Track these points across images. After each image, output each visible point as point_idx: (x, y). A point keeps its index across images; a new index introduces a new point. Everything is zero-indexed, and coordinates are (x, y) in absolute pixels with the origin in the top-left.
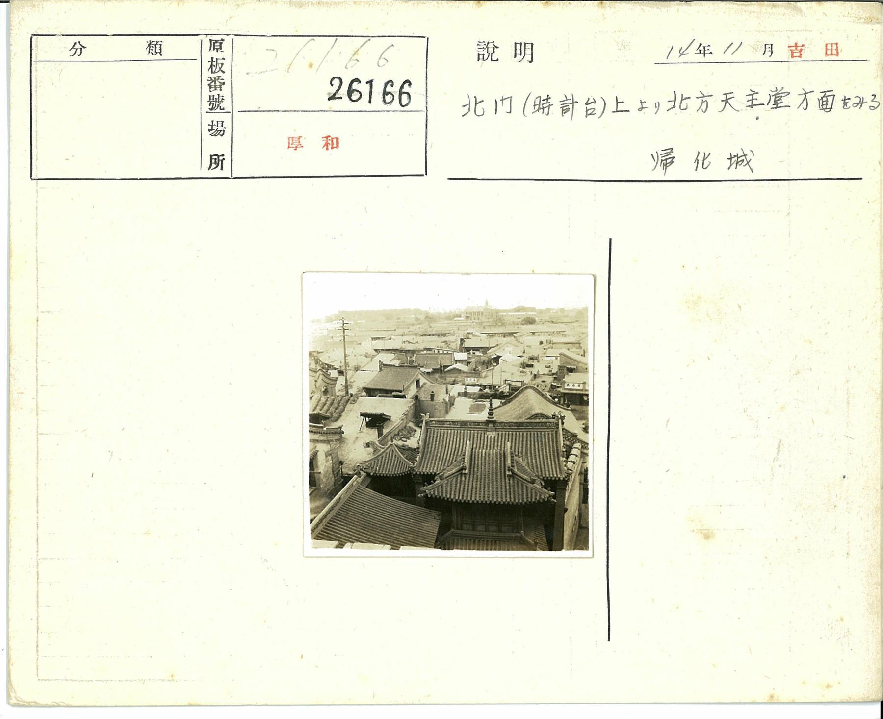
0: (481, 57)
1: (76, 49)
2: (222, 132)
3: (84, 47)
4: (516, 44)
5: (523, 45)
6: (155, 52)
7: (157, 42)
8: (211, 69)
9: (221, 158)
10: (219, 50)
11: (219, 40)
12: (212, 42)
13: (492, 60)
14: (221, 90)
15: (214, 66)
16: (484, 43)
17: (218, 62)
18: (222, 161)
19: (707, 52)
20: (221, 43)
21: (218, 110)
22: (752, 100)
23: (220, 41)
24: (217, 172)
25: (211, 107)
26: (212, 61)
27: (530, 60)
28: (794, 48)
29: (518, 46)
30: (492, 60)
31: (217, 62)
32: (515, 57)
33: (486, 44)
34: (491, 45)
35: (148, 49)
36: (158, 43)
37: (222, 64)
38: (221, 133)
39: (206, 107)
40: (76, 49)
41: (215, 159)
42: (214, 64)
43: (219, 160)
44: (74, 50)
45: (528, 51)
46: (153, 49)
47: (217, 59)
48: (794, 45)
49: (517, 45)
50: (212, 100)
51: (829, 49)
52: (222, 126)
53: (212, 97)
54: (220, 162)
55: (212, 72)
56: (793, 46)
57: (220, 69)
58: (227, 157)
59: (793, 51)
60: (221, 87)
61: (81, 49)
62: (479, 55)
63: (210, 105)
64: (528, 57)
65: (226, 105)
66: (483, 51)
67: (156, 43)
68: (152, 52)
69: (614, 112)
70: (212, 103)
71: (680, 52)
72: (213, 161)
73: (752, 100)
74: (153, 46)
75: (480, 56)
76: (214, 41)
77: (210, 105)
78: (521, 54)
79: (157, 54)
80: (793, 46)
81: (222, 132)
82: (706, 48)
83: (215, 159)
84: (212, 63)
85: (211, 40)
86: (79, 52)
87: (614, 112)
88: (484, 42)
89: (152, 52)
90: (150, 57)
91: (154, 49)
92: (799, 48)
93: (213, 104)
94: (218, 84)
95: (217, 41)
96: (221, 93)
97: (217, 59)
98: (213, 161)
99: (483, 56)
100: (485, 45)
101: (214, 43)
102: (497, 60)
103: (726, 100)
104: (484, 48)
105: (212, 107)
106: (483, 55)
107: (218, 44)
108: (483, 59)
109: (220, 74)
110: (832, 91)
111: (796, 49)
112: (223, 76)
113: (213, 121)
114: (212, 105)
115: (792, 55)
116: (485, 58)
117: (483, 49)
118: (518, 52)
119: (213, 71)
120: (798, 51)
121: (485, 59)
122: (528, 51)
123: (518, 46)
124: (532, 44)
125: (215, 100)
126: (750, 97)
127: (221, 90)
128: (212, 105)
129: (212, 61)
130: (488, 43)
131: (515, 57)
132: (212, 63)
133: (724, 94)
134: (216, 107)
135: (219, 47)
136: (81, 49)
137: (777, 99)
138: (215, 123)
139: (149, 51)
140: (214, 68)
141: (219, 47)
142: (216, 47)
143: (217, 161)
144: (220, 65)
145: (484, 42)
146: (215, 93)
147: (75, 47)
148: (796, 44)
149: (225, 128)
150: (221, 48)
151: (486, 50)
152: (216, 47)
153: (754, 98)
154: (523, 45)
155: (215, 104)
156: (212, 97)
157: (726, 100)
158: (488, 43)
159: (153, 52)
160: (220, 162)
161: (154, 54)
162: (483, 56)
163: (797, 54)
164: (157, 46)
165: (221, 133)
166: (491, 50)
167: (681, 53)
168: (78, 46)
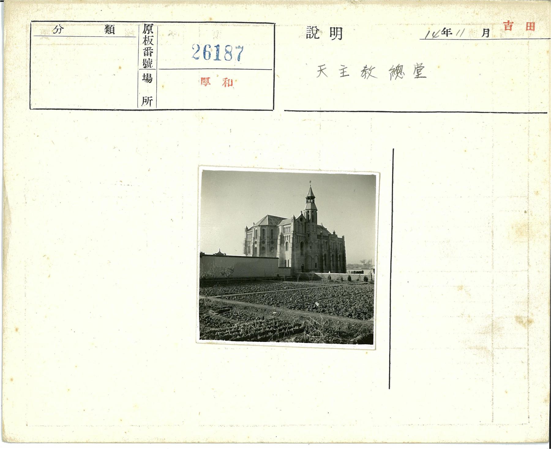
0: (308, 36)
1: (58, 29)
2: (150, 81)
3: (63, 28)
4: (331, 28)
5: (336, 29)
6: (110, 32)
7: (112, 26)
8: (144, 43)
9: (150, 99)
10: (150, 30)
11: (150, 25)
12: (146, 26)
13: (315, 38)
14: (151, 56)
15: (147, 41)
16: (310, 28)
17: (149, 38)
18: (150, 100)
19: (449, 33)
20: (151, 27)
21: (149, 68)
22: (344, 72)
23: (150, 26)
24: (147, 107)
25: (144, 66)
26: (146, 38)
27: (340, 38)
28: (507, 24)
29: (333, 30)
30: (315, 38)
31: (148, 38)
32: (331, 36)
33: (312, 28)
34: (314, 29)
35: (106, 30)
36: (112, 26)
37: (152, 39)
38: (150, 81)
39: (142, 66)
40: (58, 29)
41: (146, 99)
42: (147, 39)
43: (148, 100)
44: (56, 30)
45: (339, 33)
46: (109, 30)
47: (148, 37)
48: (507, 22)
49: (332, 29)
50: (145, 62)
51: (532, 26)
52: (150, 77)
53: (145, 60)
54: (149, 101)
55: (145, 44)
56: (506, 23)
57: (150, 43)
58: (154, 98)
59: (507, 26)
60: (151, 54)
61: (61, 29)
62: (307, 34)
63: (144, 65)
64: (339, 37)
65: (154, 65)
66: (310, 32)
67: (110, 26)
68: (108, 32)
69: (342, 76)
70: (145, 63)
71: (433, 36)
72: (145, 101)
73: (344, 72)
74: (109, 28)
75: (308, 35)
76: (147, 25)
77: (144, 65)
78: (334, 35)
79: (111, 33)
80: (506, 23)
81: (150, 81)
82: (448, 31)
83: (146, 99)
84: (145, 39)
85: (145, 25)
86: (59, 31)
87: (342, 76)
88: (310, 27)
89: (108, 32)
90: (107, 35)
91: (109, 29)
92: (510, 24)
93: (146, 64)
94: (149, 52)
95: (149, 25)
96: (151, 58)
97: (148, 37)
98: (145, 101)
99: (310, 36)
100: (311, 28)
101: (147, 26)
102: (319, 38)
103: (321, 70)
104: (310, 30)
105: (145, 66)
106: (310, 35)
107: (150, 27)
108: (310, 37)
109: (150, 45)
110: (404, 75)
111: (508, 25)
112: (153, 47)
113: (144, 74)
114: (145, 65)
115: (506, 28)
116: (311, 37)
117: (310, 31)
118: (333, 33)
119: (146, 43)
120: (509, 26)
121: (311, 37)
122: (339, 33)
123: (333, 30)
124: (341, 28)
125: (147, 61)
126: (342, 71)
127: (151, 56)
128: (145, 65)
129: (146, 38)
130: (313, 27)
131: (331, 36)
132: (145, 39)
133: (215, 47)
134: (148, 66)
135: (150, 29)
136: (61, 29)
137: (418, 71)
138: (146, 75)
139: (106, 31)
140: (146, 42)
141: (150, 29)
142: (148, 29)
143: (147, 100)
144: (151, 40)
145: (310, 27)
146: (147, 58)
147: (57, 28)
148: (509, 21)
149: (152, 78)
150: (151, 30)
151: (311, 32)
152: (148, 29)
153: (344, 71)
154: (336, 29)
155: (147, 64)
156: (145, 60)
157: (321, 70)
158: (313, 27)
159: (109, 32)
160: (149, 101)
161: (110, 33)
162: (310, 36)
163: (508, 28)
164: (111, 28)
165: (150, 81)
166: (314, 32)
167: (434, 35)
168: (59, 27)
